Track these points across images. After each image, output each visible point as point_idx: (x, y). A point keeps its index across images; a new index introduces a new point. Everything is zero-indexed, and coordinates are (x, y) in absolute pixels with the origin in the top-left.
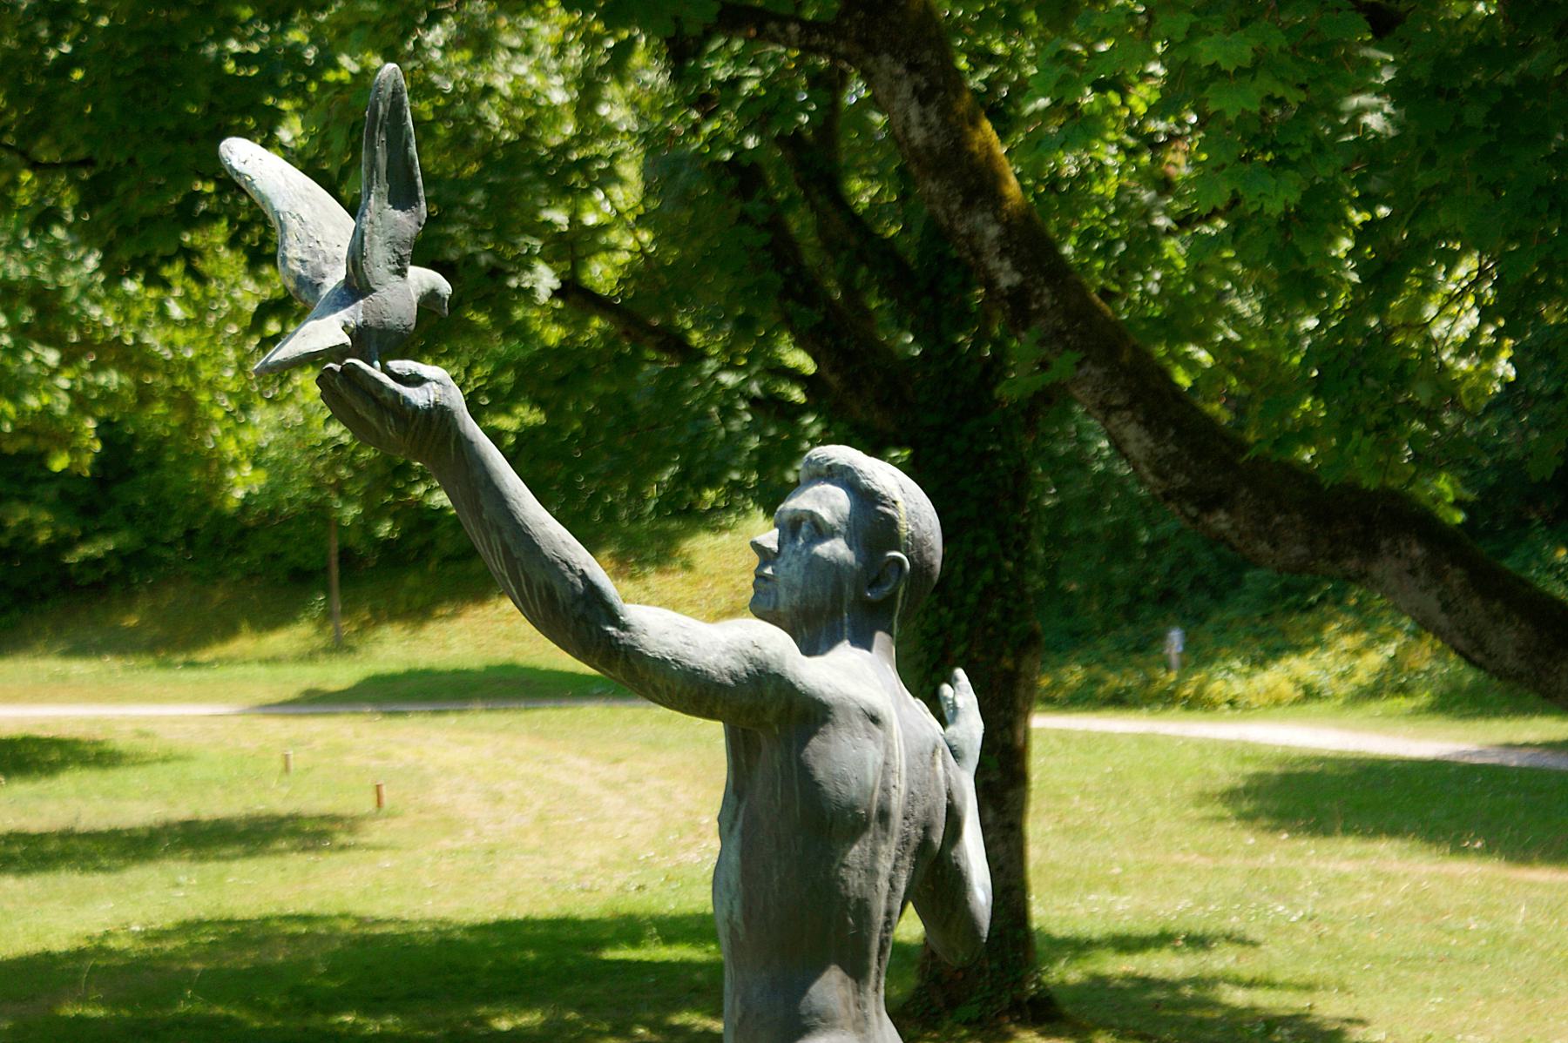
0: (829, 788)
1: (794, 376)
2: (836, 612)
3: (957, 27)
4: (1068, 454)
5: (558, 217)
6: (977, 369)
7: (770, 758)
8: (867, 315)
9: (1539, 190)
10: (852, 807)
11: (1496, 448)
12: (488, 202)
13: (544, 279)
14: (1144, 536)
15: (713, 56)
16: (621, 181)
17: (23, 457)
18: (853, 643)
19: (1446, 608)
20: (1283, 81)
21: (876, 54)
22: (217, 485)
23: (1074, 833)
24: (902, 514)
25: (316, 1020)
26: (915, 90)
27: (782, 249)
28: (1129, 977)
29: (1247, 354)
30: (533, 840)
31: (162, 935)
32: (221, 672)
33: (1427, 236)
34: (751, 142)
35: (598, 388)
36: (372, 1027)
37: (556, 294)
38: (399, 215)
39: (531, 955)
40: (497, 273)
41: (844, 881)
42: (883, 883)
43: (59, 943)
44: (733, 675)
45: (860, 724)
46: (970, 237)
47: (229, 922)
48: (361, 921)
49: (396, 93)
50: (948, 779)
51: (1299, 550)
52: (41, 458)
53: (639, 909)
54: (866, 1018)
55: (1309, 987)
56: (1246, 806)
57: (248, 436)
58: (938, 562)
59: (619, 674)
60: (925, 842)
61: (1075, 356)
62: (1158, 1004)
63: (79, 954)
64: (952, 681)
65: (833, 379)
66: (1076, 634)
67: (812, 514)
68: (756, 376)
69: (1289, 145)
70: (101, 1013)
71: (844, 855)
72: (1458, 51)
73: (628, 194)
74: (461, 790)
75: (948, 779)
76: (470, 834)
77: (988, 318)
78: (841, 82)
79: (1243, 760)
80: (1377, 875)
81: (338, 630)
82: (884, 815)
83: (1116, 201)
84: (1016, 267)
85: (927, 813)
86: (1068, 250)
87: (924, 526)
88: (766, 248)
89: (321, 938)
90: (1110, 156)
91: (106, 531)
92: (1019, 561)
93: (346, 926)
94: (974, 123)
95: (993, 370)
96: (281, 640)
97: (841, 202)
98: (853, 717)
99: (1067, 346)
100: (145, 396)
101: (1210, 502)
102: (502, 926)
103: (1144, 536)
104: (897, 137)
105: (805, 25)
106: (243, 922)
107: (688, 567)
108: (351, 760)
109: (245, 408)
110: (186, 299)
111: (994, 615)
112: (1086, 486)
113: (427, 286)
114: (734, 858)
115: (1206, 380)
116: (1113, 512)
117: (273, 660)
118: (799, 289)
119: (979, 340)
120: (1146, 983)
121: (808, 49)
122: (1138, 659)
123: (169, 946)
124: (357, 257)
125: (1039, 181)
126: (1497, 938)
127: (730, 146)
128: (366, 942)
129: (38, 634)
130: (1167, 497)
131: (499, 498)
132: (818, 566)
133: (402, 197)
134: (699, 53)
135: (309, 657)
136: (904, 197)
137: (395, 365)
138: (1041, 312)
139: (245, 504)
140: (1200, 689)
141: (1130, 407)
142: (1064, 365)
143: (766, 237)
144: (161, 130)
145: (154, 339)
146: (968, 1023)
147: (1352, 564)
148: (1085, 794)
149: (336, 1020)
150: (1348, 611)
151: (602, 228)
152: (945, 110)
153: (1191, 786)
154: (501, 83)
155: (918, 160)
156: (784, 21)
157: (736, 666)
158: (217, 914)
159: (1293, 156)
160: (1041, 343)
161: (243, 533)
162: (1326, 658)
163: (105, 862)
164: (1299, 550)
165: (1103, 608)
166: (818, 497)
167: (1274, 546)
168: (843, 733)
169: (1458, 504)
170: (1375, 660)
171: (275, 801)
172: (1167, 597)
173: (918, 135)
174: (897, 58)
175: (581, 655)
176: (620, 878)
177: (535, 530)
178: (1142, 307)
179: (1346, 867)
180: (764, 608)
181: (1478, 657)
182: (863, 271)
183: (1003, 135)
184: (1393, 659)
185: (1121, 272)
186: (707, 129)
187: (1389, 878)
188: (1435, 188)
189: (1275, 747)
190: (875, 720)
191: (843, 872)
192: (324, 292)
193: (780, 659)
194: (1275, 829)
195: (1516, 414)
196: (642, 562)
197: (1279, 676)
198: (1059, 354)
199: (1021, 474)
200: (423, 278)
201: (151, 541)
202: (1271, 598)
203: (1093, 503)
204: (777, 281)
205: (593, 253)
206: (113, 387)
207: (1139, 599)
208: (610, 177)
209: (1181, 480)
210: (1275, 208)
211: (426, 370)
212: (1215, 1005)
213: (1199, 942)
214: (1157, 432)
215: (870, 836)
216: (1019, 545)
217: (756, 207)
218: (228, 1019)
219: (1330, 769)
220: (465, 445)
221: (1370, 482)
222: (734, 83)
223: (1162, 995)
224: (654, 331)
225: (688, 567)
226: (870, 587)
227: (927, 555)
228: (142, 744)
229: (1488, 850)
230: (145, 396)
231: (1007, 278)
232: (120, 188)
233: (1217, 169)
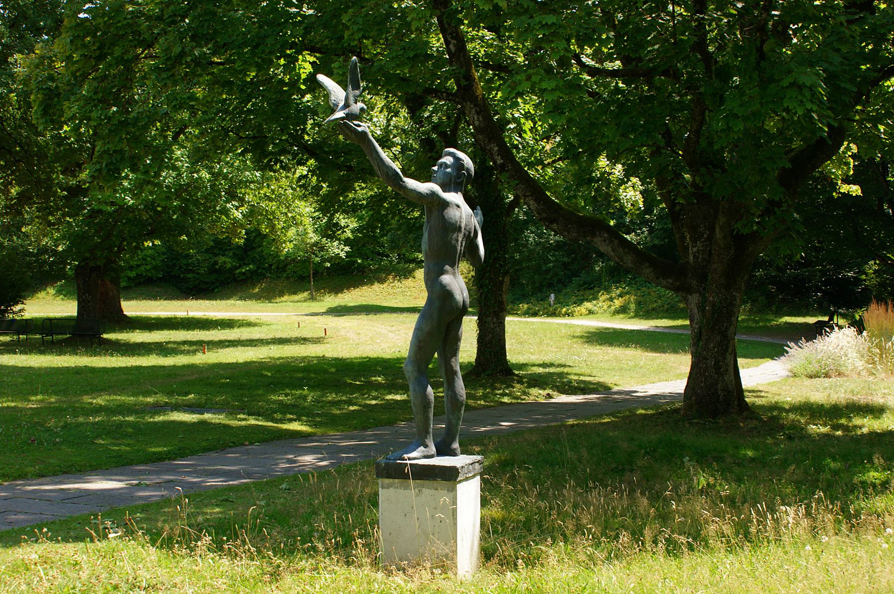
2: (450, 184)
20: (562, 92)
45: (455, 207)
46: (490, 150)
51: (575, 234)
66: (524, 296)
74: (348, 332)
82: (460, 227)
107: (414, 278)
108: (317, 325)
122: (542, 302)
124: (347, 99)
130: (540, 220)
137: (355, 122)
139: (287, 257)
141: (531, 196)
147: (588, 238)
164: (575, 234)
167: (568, 233)
201: (258, 268)
216: (504, 247)
225: (414, 278)
228: (258, 321)
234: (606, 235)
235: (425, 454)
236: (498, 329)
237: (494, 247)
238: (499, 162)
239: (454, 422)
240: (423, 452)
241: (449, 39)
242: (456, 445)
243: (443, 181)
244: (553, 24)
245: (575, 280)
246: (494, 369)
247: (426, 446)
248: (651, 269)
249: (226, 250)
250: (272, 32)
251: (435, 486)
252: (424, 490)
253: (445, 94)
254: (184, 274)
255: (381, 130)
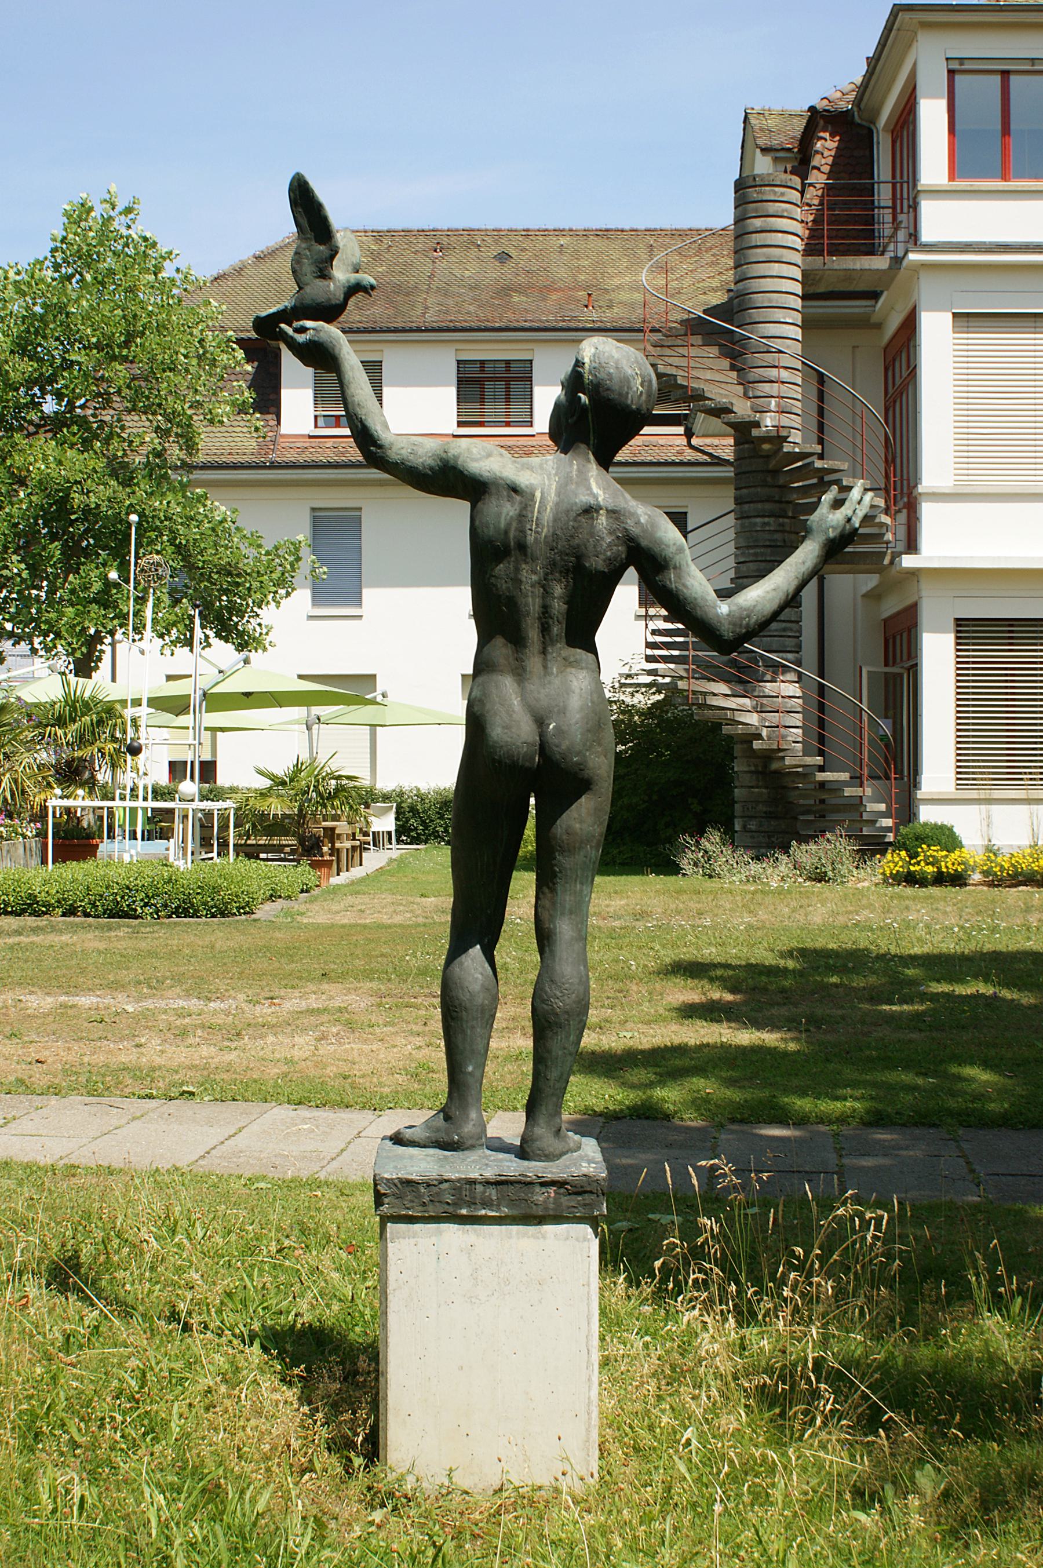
38: (322, 248)
41: (495, 586)
71: (493, 570)
98: (501, 489)
215: (513, 559)
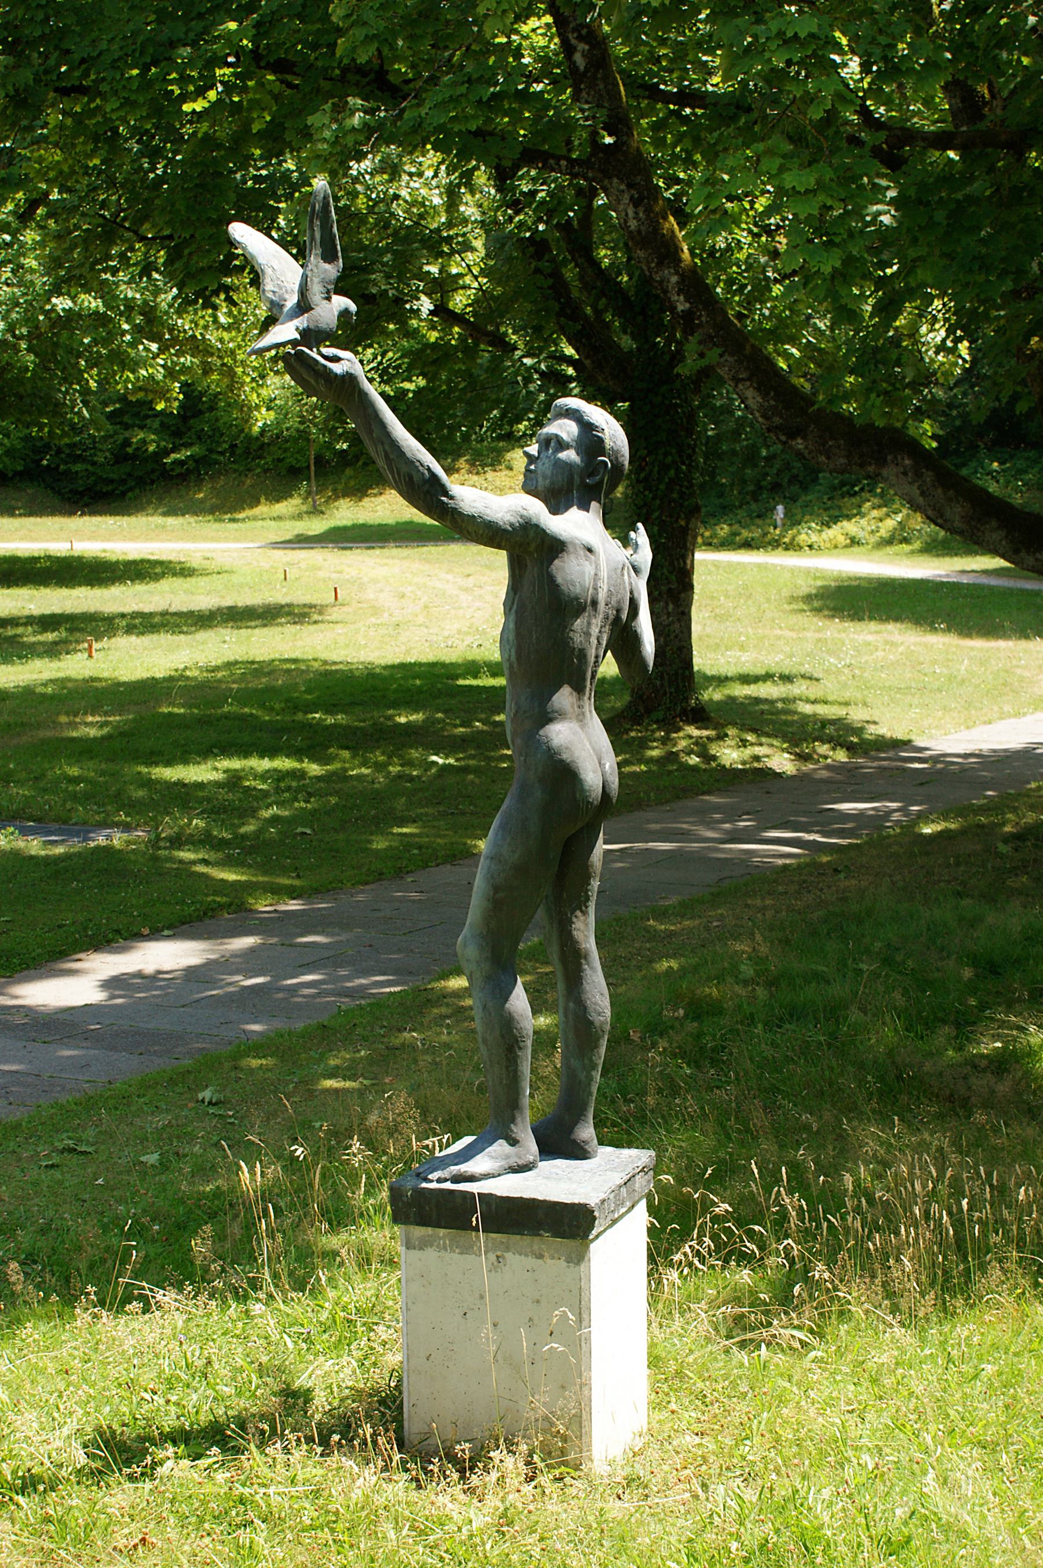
0: (564, 588)
1: (569, 361)
2: (569, 491)
3: (658, 164)
4: (722, 406)
5: (434, 269)
6: (667, 357)
7: (532, 571)
8: (608, 326)
9: (974, 258)
10: (577, 599)
11: (961, 405)
12: (394, 260)
13: (426, 304)
14: (764, 453)
15: (521, 178)
16: (473, 250)
17: (140, 403)
18: (579, 508)
19: (923, 494)
20: (832, 196)
21: (610, 178)
22: (247, 420)
23: (721, 618)
24: (607, 437)
25: (300, 716)
26: (632, 198)
27: (560, 287)
28: (748, 697)
29: (820, 350)
30: (421, 619)
31: (216, 669)
32: (249, 524)
33: (914, 285)
34: (541, 227)
35: (604, 384)
36: (330, 720)
37: (432, 313)
38: (327, 266)
39: (418, 682)
40: (399, 301)
42: (594, 641)
43: (160, 673)
44: (511, 525)
46: (661, 282)
47: (253, 662)
48: (325, 662)
49: (325, 198)
50: (631, 584)
51: (842, 461)
52: (150, 405)
53: (478, 658)
54: (583, 714)
55: (847, 704)
56: (816, 604)
57: (264, 392)
58: (626, 463)
59: (448, 524)
60: (617, 618)
61: (720, 351)
62: (762, 712)
63: (171, 679)
64: (635, 530)
65: (587, 362)
66: (725, 507)
67: (557, 436)
68: (545, 359)
69: (834, 234)
70: (182, 711)
72: (931, 180)
73: (477, 254)
74: (382, 591)
75: (631, 584)
76: (386, 615)
77: (674, 330)
78: (594, 194)
79: (815, 578)
80: (886, 642)
81: (314, 501)
82: (594, 603)
83: (746, 262)
84: (687, 300)
85: (619, 602)
86: (719, 290)
87: (619, 443)
88: (550, 288)
89: (303, 671)
90: (744, 238)
91: (187, 445)
92: (689, 466)
93: (316, 665)
94: (665, 218)
95: (678, 357)
96: (282, 507)
97: (595, 263)
99: (715, 345)
100: (207, 369)
101: (793, 433)
102: (402, 666)
103: (764, 453)
104: (624, 225)
105: (572, 162)
106: (259, 662)
108: (321, 574)
109: (263, 377)
110: (229, 314)
111: (675, 495)
112: (732, 425)
113: (343, 306)
114: (512, 626)
115: (796, 365)
116: (747, 439)
117: (279, 518)
118: (569, 311)
119: (668, 342)
120: (757, 701)
121: (575, 176)
122: (759, 522)
123: (220, 675)
124: (304, 290)
125: (703, 251)
126: (951, 678)
127: (529, 229)
128: (327, 674)
129: (149, 503)
131: (382, 425)
132: (559, 464)
133: (329, 257)
134: (513, 176)
135: (299, 517)
136: (629, 259)
137: (325, 351)
138: (701, 325)
139: (263, 431)
140: (793, 539)
141: (749, 379)
142: (713, 355)
143: (550, 281)
144: (209, 218)
145: (212, 337)
146: (657, 722)
147: (871, 469)
148: (727, 596)
149: (310, 716)
150: (875, 496)
151: (460, 276)
152: (648, 210)
153: (786, 593)
154: (404, 193)
155: (632, 238)
156: (559, 159)
157: (513, 520)
158: (245, 658)
159: (837, 240)
160: (700, 343)
161: (262, 446)
162: (863, 522)
163: (185, 629)
164: (842, 461)
165: (740, 493)
166: (560, 427)
167: (828, 458)
168: (572, 557)
169: (934, 437)
170: (890, 523)
171: (279, 596)
172: (776, 487)
173: (633, 224)
174: (621, 180)
175: (428, 512)
176: (468, 640)
177: (402, 443)
178: (761, 323)
179: (870, 638)
180: (530, 489)
181: (939, 521)
182: (603, 301)
183: (682, 225)
184: (900, 523)
185: (749, 303)
186: (517, 219)
187: (893, 644)
188: (918, 259)
189: (832, 571)
190: (590, 550)
191: (571, 634)
192: (285, 310)
193: (538, 516)
194: (833, 617)
195: (972, 387)
196: (483, 466)
197: (837, 532)
198: (710, 349)
199: (691, 416)
200: (341, 302)
201: (211, 451)
202: (834, 488)
203: (736, 434)
204: (557, 307)
205: (455, 290)
206: (188, 364)
207: (761, 488)
208: (467, 247)
209: (777, 420)
210: (827, 269)
211: (341, 353)
212: (796, 713)
213: (787, 678)
214: (765, 395)
216: (689, 457)
217: (544, 265)
218: (252, 715)
219: (864, 584)
220: (363, 395)
221: (880, 423)
222: (533, 193)
223: (765, 707)
224: (487, 334)
226: (589, 477)
227: (621, 459)
228: (206, 564)
229: (949, 630)
230: (207, 369)
231: (682, 306)
232: (186, 252)
233: (795, 247)
234: (907, 462)
235: (513, 1161)
236: (677, 625)
237: (669, 459)
238: (680, 308)
239: (582, 1076)
240: (507, 1157)
241: (573, 42)
242: (587, 1132)
243: (552, 483)
244: (812, 35)
245: (824, 478)
246: (669, 709)
247: (513, 1142)
248: (1002, 533)
249: (147, 417)
250: (186, 33)
251: (536, 1247)
252: (509, 1255)
253: (563, 163)
254: (66, 463)
255: (441, 194)
